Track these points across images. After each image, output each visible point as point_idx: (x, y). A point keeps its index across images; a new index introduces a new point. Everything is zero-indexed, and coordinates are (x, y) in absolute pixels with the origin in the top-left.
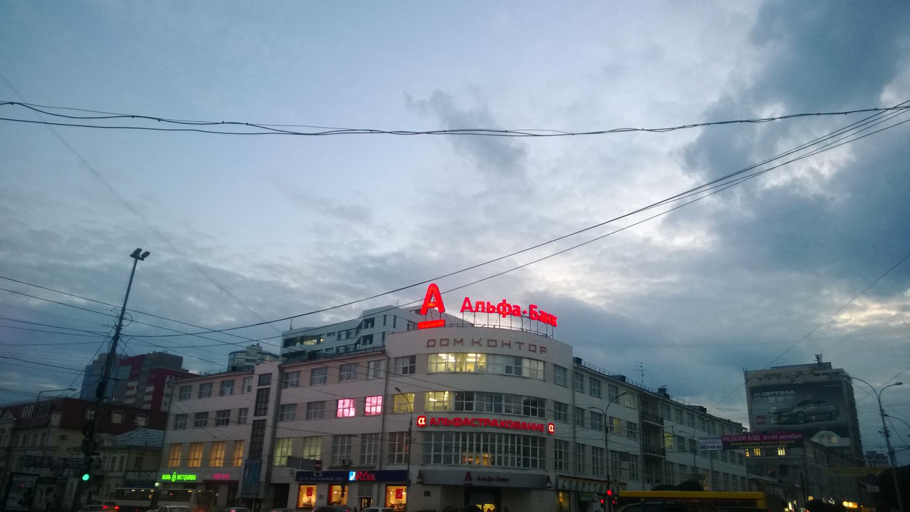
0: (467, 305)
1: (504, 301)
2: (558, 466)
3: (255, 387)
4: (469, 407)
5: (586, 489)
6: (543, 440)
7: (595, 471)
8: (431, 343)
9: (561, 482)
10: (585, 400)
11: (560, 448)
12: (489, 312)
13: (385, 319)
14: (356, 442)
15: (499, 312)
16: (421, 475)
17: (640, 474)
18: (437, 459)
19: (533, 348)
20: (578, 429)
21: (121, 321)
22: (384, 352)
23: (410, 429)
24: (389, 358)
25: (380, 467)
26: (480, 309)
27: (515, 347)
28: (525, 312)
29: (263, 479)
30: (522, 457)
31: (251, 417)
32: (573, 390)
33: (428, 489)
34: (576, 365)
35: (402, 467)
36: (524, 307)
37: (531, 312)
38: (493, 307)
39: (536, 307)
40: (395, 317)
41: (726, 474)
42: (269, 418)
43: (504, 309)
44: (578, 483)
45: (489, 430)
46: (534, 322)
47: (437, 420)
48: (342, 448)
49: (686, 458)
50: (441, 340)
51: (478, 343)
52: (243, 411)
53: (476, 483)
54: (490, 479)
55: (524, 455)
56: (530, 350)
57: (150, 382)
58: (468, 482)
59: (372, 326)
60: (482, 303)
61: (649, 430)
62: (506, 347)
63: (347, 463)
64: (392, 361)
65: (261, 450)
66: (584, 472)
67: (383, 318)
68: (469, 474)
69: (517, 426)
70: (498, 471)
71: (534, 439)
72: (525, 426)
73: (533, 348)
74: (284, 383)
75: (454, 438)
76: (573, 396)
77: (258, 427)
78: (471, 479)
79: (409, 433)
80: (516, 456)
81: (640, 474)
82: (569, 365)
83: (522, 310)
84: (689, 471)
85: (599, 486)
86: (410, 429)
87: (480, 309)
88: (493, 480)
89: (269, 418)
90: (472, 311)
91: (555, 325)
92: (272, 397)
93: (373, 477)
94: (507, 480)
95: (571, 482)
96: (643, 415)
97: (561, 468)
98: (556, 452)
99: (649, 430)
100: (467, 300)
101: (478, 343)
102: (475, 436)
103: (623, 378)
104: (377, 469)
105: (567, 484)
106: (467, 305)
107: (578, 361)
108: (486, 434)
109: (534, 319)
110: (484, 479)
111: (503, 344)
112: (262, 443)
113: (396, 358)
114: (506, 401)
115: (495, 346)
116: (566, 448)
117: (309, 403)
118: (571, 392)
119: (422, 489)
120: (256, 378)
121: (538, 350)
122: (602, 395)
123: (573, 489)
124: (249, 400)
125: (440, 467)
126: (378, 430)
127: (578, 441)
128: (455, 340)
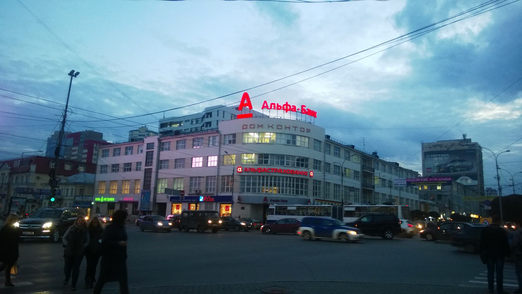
0: (265, 105)
1: (287, 103)
2: (315, 194)
6: (307, 180)
7: (335, 196)
8: (245, 127)
12: (278, 109)
13: (218, 113)
14: (203, 180)
15: (284, 109)
16: (239, 198)
18: (248, 190)
19: (302, 130)
24: (221, 135)
26: (273, 108)
27: (292, 129)
28: (298, 109)
30: (295, 189)
31: (143, 167)
33: (243, 206)
34: (326, 139)
36: (298, 107)
37: (302, 109)
38: (280, 106)
39: (305, 106)
43: (287, 107)
45: (277, 174)
46: (304, 115)
48: (196, 184)
50: (251, 125)
51: (271, 127)
52: (139, 164)
56: (301, 131)
58: (265, 202)
59: (211, 116)
60: (274, 104)
61: (366, 175)
63: (198, 192)
65: (150, 185)
69: (292, 172)
71: (302, 180)
73: (302, 130)
76: (324, 157)
77: (148, 172)
79: (233, 176)
80: (292, 189)
81: (360, 198)
82: (323, 139)
83: (297, 108)
87: (273, 108)
89: (154, 167)
90: (268, 109)
91: (316, 117)
92: (155, 156)
93: (213, 199)
96: (363, 167)
97: (316, 195)
99: (366, 175)
100: (265, 102)
101: (271, 127)
102: (273, 178)
103: (353, 147)
104: (215, 195)
106: (265, 105)
107: (328, 137)
108: (275, 177)
109: (303, 113)
111: (286, 128)
113: (225, 135)
114: (287, 159)
117: (176, 160)
119: (240, 206)
121: (306, 131)
124: (142, 158)
125: (250, 194)
126: (216, 174)
127: (326, 181)
128: (258, 125)
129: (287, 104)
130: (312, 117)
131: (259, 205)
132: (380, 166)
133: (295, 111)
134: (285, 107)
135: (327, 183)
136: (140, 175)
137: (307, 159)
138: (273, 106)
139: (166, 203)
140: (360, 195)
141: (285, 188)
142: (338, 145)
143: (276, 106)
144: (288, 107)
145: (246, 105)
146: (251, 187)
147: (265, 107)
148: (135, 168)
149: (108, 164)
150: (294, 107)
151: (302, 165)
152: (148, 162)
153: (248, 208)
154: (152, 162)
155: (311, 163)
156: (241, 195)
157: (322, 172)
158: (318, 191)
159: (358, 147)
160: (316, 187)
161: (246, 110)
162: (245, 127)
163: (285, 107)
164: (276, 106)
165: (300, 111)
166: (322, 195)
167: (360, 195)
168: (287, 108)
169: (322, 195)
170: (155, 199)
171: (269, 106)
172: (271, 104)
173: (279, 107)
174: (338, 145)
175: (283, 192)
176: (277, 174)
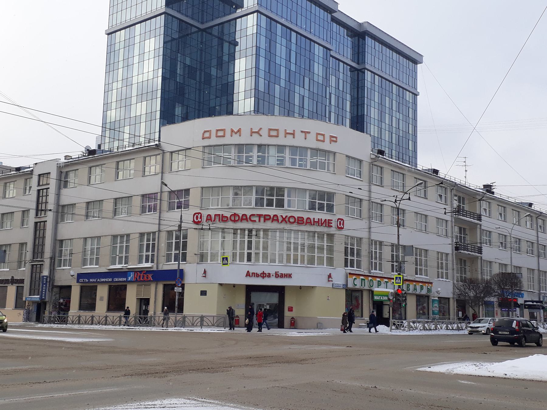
3: (35, 188)
4: (280, 204)
6: (331, 237)
8: (207, 135)
9: (350, 280)
14: (107, 241)
17: (450, 272)
19: (320, 138)
20: (375, 224)
21: (370, 194)
24: (164, 152)
25: (157, 268)
27: (300, 137)
31: (32, 218)
47: (213, 217)
50: (217, 131)
51: (257, 133)
52: (25, 212)
56: (317, 140)
64: (168, 155)
73: (320, 138)
77: (39, 229)
81: (450, 272)
88: (269, 275)
89: (50, 217)
92: (51, 199)
93: (150, 276)
101: (257, 133)
102: (247, 232)
103: (436, 172)
104: (155, 269)
105: (358, 283)
111: (287, 133)
113: (172, 153)
114: (289, 196)
115: (277, 136)
117: (88, 203)
120: (35, 179)
121: (327, 139)
126: (155, 228)
127: (374, 237)
128: (232, 131)
136: (27, 235)
139: (70, 287)
140: (450, 266)
142: (500, 202)
148: (384, 248)
149: (524, 255)
151: (321, 208)
155: (338, 202)
158: (246, 251)
162: (207, 135)
167: (450, 266)
174: (500, 202)
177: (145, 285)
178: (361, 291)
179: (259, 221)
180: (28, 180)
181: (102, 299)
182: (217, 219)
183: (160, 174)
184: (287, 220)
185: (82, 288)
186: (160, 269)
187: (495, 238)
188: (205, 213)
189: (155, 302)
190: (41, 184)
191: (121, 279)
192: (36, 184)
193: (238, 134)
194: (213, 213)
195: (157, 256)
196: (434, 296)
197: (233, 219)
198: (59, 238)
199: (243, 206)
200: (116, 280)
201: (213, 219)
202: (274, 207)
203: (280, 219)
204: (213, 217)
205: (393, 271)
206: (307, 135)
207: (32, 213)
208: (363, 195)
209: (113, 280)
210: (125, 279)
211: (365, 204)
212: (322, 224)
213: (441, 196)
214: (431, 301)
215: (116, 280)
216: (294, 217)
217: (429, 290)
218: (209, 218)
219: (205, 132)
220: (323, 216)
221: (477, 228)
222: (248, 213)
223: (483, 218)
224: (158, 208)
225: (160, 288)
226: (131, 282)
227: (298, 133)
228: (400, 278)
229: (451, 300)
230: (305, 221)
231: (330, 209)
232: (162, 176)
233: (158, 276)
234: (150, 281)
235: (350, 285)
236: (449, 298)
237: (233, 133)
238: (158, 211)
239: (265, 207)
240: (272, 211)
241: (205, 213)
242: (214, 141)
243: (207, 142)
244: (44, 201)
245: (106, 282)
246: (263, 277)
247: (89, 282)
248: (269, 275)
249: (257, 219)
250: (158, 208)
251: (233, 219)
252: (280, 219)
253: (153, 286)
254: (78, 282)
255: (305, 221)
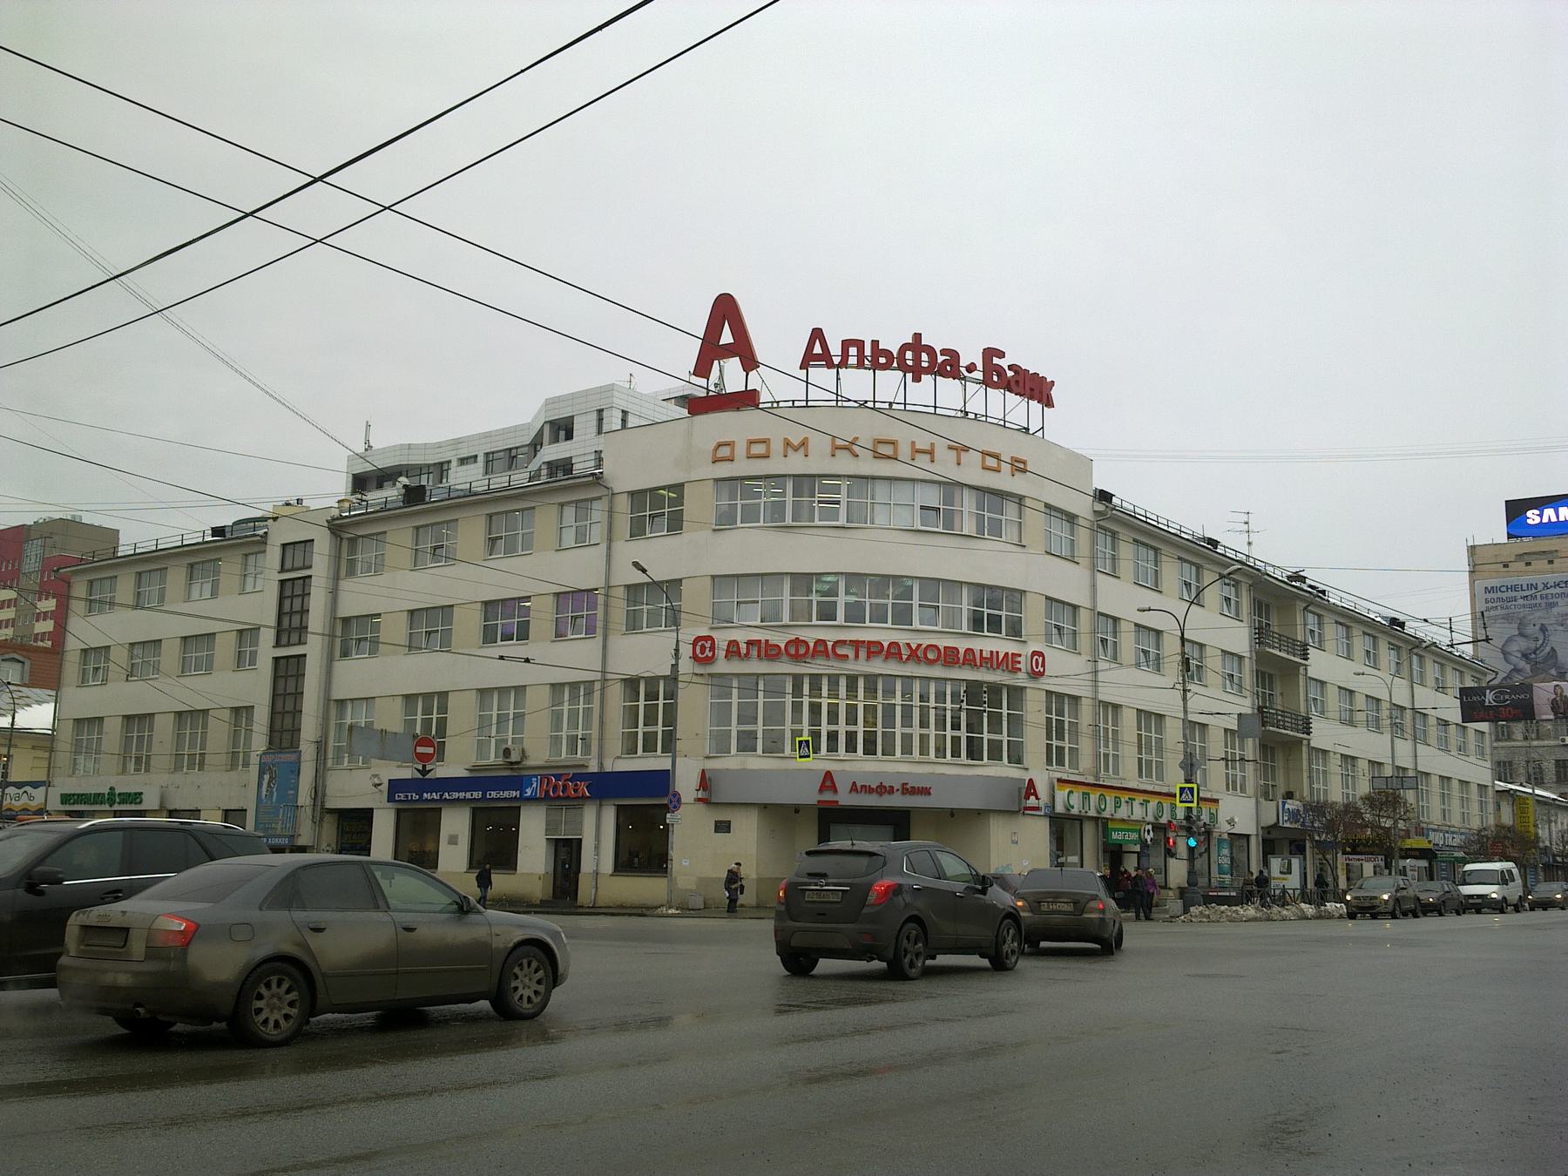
0: (817, 349)
1: (917, 336)
2: (1054, 756)
4: (827, 613)
5: (1123, 813)
6: (1017, 693)
7: (1143, 768)
10: (1122, 598)
11: (1060, 713)
12: (876, 366)
13: (600, 420)
15: (903, 367)
16: (705, 782)
18: (747, 743)
19: (991, 462)
22: (597, 480)
23: (675, 667)
26: (853, 360)
27: (944, 455)
28: (971, 368)
29: (304, 797)
30: (963, 734)
32: (1094, 569)
33: (723, 816)
34: (1100, 507)
35: (663, 763)
36: (970, 355)
37: (989, 368)
38: (887, 354)
39: (1001, 355)
40: (625, 413)
41: (1445, 780)
42: (313, 649)
43: (917, 359)
44: (1102, 798)
45: (878, 667)
46: (995, 395)
48: (502, 719)
49: (1370, 745)
50: (751, 442)
52: (247, 635)
53: (845, 799)
54: (882, 790)
55: (970, 728)
57: (43, 593)
58: (828, 796)
59: (569, 436)
60: (859, 344)
61: (1275, 670)
62: (923, 460)
63: (514, 757)
65: (296, 731)
66: (1116, 772)
67: (594, 416)
68: (828, 774)
69: (950, 657)
70: (904, 768)
71: (995, 689)
72: (970, 659)
74: (344, 567)
75: (789, 689)
76: (1094, 586)
77: (288, 673)
78: (834, 789)
79: (673, 679)
80: (949, 733)
82: (1083, 507)
83: (964, 362)
84: (1388, 771)
85: (1153, 805)
86: (675, 667)
87: (853, 360)
88: (891, 790)
90: (830, 365)
91: (1049, 403)
93: (583, 786)
94: (925, 791)
95: (1086, 796)
96: (1261, 634)
97: (1060, 762)
98: (1049, 720)
99: (1275, 670)
100: (817, 334)
102: (843, 683)
103: (1214, 543)
104: (593, 767)
105: (1076, 800)
106: (817, 349)
107: (1104, 496)
108: (871, 680)
109: (996, 386)
110: (868, 790)
112: (297, 712)
116: (1075, 713)
118: (1087, 573)
119: (709, 818)
120: (273, 554)
122: (1164, 586)
123: (1092, 813)
124: (260, 606)
125: (757, 762)
127: (1105, 695)
129: (917, 345)
130: (1035, 406)
131: (797, 809)
132: (1331, 631)
133: (956, 374)
134: (909, 355)
135: (1106, 705)
136: (256, 688)
137: (1017, 596)
138: (853, 351)
141: (916, 731)
143: (868, 352)
144: (924, 357)
145: (728, 352)
146: (734, 729)
147: (818, 357)
150: (953, 355)
152: (290, 623)
153: (747, 828)
154: (303, 628)
155: (1034, 617)
156: (711, 765)
157: (1085, 657)
159: (1233, 543)
160: (1060, 723)
161: (731, 374)
163: (909, 355)
164: (868, 352)
165: (978, 375)
166: (1086, 762)
168: (921, 359)
169: (1086, 762)
170: (318, 792)
171: (835, 350)
172: (846, 344)
173: (878, 359)
175: (907, 749)
176: (863, 666)
177: (568, 807)
178: (1080, 819)
179: (857, 656)
180: (251, 559)
181: (453, 840)
182: (754, 652)
183: (604, 546)
184: (920, 653)
185: (398, 812)
186: (609, 767)
187: (1333, 699)
188: (722, 638)
189: (597, 847)
190: (288, 565)
191: (506, 794)
192: (278, 567)
193: (802, 450)
194: (741, 637)
195: (601, 739)
196: (1223, 828)
197: (792, 651)
198: (338, 694)
199: (814, 622)
200: (494, 794)
201: (743, 651)
202: (889, 625)
203: (905, 653)
204: (743, 647)
205: (1140, 776)
206: (963, 454)
207: (267, 637)
208: (1080, 597)
209: (484, 795)
210: (514, 794)
211: (1084, 617)
212: (999, 665)
213: (1228, 600)
214: (1214, 842)
215: (494, 794)
216: (936, 647)
217: (1214, 817)
218: (733, 650)
219: (720, 445)
220: (998, 645)
221: (1297, 675)
222: (830, 636)
223: (1311, 651)
224: (600, 624)
225: (610, 816)
226: (533, 800)
227: (941, 451)
228: (1191, 790)
229: (1253, 841)
230: (961, 656)
231: (1015, 631)
232: (609, 548)
233: (604, 786)
234: (584, 797)
235: (1059, 809)
236: (1248, 836)
237: (790, 451)
238: (599, 631)
239: (867, 624)
240: (885, 634)
241: (722, 638)
242: (742, 467)
243: (724, 470)
244: (297, 607)
245: (465, 799)
246: (881, 794)
247: (421, 800)
248: (891, 790)
249: (850, 652)
250: (600, 624)
251: (792, 651)
252: (905, 653)
253: (589, 814)
254: (391, 799)
255: (961, 656)
